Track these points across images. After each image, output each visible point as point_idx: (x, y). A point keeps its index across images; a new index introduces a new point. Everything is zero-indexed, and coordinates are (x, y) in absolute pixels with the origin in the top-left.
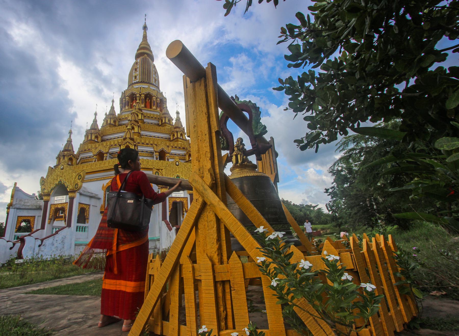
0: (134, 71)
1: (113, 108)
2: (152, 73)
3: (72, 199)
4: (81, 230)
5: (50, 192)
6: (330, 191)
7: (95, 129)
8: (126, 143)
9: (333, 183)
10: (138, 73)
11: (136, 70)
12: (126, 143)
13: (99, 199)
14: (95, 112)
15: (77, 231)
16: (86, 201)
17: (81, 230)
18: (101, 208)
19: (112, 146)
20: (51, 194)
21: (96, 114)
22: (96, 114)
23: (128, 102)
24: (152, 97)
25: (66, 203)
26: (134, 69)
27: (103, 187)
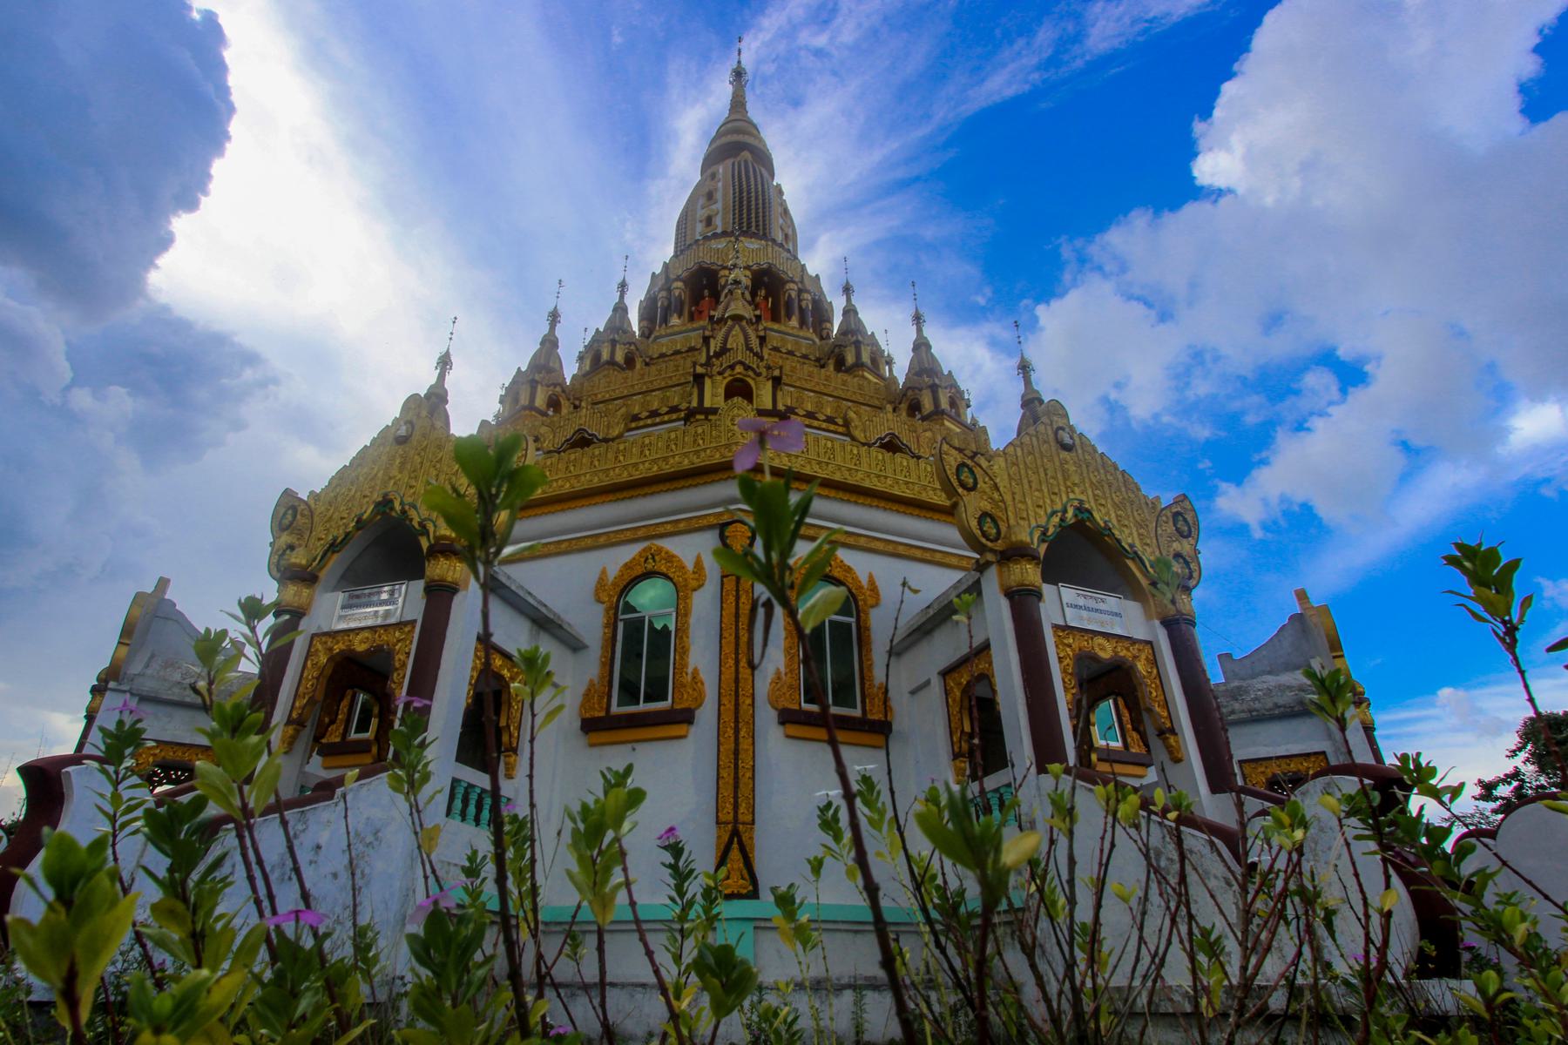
0: (702, 201)
1: (621, 309)
2: (776, 210)
3: (440, 596)
4: (472, 809)
5: (321, 566)
6: (1504, 791)
7: (550, 371)
8: (732, 367)
9: (1513, 753)
10: (719, 206)
11: (710, 196)
12: (732, 367)
13: (575, 645)
14: (551, 308)
15: (448, 813)
16: (513, 635)
17: (472, 809)
18: (587, 695)
19: (636, 418)
20: (322, 575)
21: (554, 317)
22: (554, 317)
23: (682, 304)
24: (784, 282)
25: (400, 625)
26: (704, 194)
27: (601, 583)
